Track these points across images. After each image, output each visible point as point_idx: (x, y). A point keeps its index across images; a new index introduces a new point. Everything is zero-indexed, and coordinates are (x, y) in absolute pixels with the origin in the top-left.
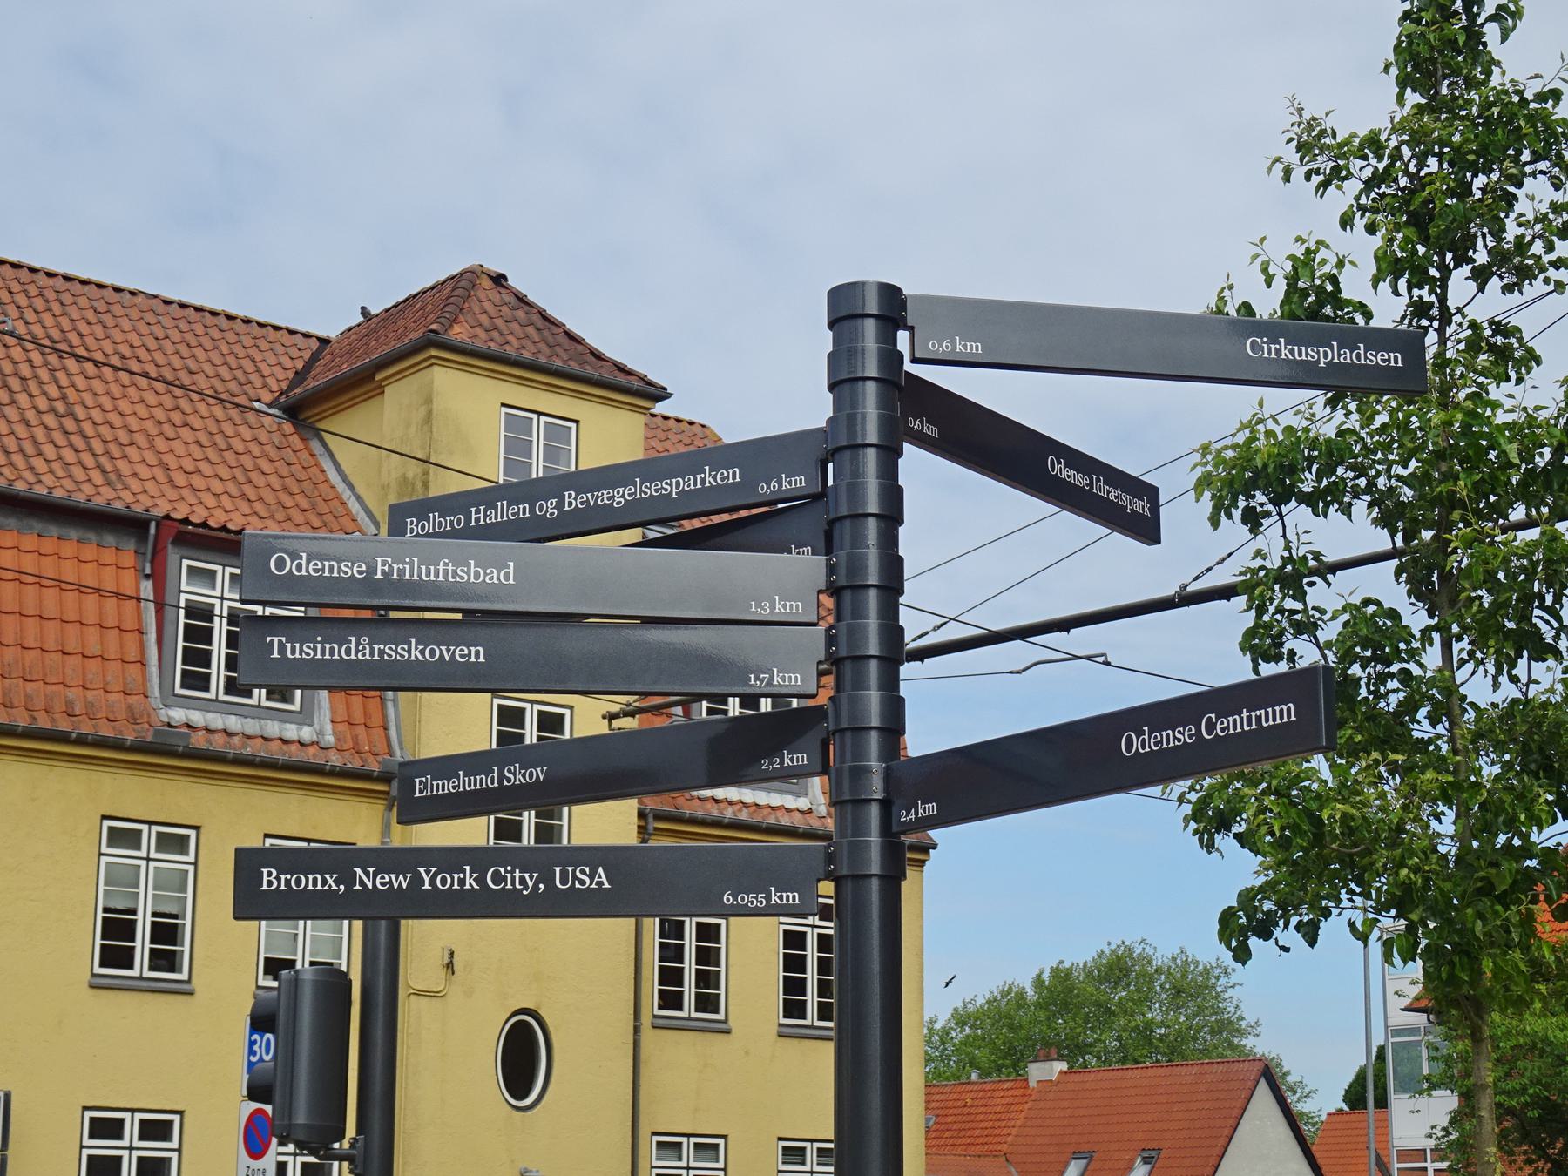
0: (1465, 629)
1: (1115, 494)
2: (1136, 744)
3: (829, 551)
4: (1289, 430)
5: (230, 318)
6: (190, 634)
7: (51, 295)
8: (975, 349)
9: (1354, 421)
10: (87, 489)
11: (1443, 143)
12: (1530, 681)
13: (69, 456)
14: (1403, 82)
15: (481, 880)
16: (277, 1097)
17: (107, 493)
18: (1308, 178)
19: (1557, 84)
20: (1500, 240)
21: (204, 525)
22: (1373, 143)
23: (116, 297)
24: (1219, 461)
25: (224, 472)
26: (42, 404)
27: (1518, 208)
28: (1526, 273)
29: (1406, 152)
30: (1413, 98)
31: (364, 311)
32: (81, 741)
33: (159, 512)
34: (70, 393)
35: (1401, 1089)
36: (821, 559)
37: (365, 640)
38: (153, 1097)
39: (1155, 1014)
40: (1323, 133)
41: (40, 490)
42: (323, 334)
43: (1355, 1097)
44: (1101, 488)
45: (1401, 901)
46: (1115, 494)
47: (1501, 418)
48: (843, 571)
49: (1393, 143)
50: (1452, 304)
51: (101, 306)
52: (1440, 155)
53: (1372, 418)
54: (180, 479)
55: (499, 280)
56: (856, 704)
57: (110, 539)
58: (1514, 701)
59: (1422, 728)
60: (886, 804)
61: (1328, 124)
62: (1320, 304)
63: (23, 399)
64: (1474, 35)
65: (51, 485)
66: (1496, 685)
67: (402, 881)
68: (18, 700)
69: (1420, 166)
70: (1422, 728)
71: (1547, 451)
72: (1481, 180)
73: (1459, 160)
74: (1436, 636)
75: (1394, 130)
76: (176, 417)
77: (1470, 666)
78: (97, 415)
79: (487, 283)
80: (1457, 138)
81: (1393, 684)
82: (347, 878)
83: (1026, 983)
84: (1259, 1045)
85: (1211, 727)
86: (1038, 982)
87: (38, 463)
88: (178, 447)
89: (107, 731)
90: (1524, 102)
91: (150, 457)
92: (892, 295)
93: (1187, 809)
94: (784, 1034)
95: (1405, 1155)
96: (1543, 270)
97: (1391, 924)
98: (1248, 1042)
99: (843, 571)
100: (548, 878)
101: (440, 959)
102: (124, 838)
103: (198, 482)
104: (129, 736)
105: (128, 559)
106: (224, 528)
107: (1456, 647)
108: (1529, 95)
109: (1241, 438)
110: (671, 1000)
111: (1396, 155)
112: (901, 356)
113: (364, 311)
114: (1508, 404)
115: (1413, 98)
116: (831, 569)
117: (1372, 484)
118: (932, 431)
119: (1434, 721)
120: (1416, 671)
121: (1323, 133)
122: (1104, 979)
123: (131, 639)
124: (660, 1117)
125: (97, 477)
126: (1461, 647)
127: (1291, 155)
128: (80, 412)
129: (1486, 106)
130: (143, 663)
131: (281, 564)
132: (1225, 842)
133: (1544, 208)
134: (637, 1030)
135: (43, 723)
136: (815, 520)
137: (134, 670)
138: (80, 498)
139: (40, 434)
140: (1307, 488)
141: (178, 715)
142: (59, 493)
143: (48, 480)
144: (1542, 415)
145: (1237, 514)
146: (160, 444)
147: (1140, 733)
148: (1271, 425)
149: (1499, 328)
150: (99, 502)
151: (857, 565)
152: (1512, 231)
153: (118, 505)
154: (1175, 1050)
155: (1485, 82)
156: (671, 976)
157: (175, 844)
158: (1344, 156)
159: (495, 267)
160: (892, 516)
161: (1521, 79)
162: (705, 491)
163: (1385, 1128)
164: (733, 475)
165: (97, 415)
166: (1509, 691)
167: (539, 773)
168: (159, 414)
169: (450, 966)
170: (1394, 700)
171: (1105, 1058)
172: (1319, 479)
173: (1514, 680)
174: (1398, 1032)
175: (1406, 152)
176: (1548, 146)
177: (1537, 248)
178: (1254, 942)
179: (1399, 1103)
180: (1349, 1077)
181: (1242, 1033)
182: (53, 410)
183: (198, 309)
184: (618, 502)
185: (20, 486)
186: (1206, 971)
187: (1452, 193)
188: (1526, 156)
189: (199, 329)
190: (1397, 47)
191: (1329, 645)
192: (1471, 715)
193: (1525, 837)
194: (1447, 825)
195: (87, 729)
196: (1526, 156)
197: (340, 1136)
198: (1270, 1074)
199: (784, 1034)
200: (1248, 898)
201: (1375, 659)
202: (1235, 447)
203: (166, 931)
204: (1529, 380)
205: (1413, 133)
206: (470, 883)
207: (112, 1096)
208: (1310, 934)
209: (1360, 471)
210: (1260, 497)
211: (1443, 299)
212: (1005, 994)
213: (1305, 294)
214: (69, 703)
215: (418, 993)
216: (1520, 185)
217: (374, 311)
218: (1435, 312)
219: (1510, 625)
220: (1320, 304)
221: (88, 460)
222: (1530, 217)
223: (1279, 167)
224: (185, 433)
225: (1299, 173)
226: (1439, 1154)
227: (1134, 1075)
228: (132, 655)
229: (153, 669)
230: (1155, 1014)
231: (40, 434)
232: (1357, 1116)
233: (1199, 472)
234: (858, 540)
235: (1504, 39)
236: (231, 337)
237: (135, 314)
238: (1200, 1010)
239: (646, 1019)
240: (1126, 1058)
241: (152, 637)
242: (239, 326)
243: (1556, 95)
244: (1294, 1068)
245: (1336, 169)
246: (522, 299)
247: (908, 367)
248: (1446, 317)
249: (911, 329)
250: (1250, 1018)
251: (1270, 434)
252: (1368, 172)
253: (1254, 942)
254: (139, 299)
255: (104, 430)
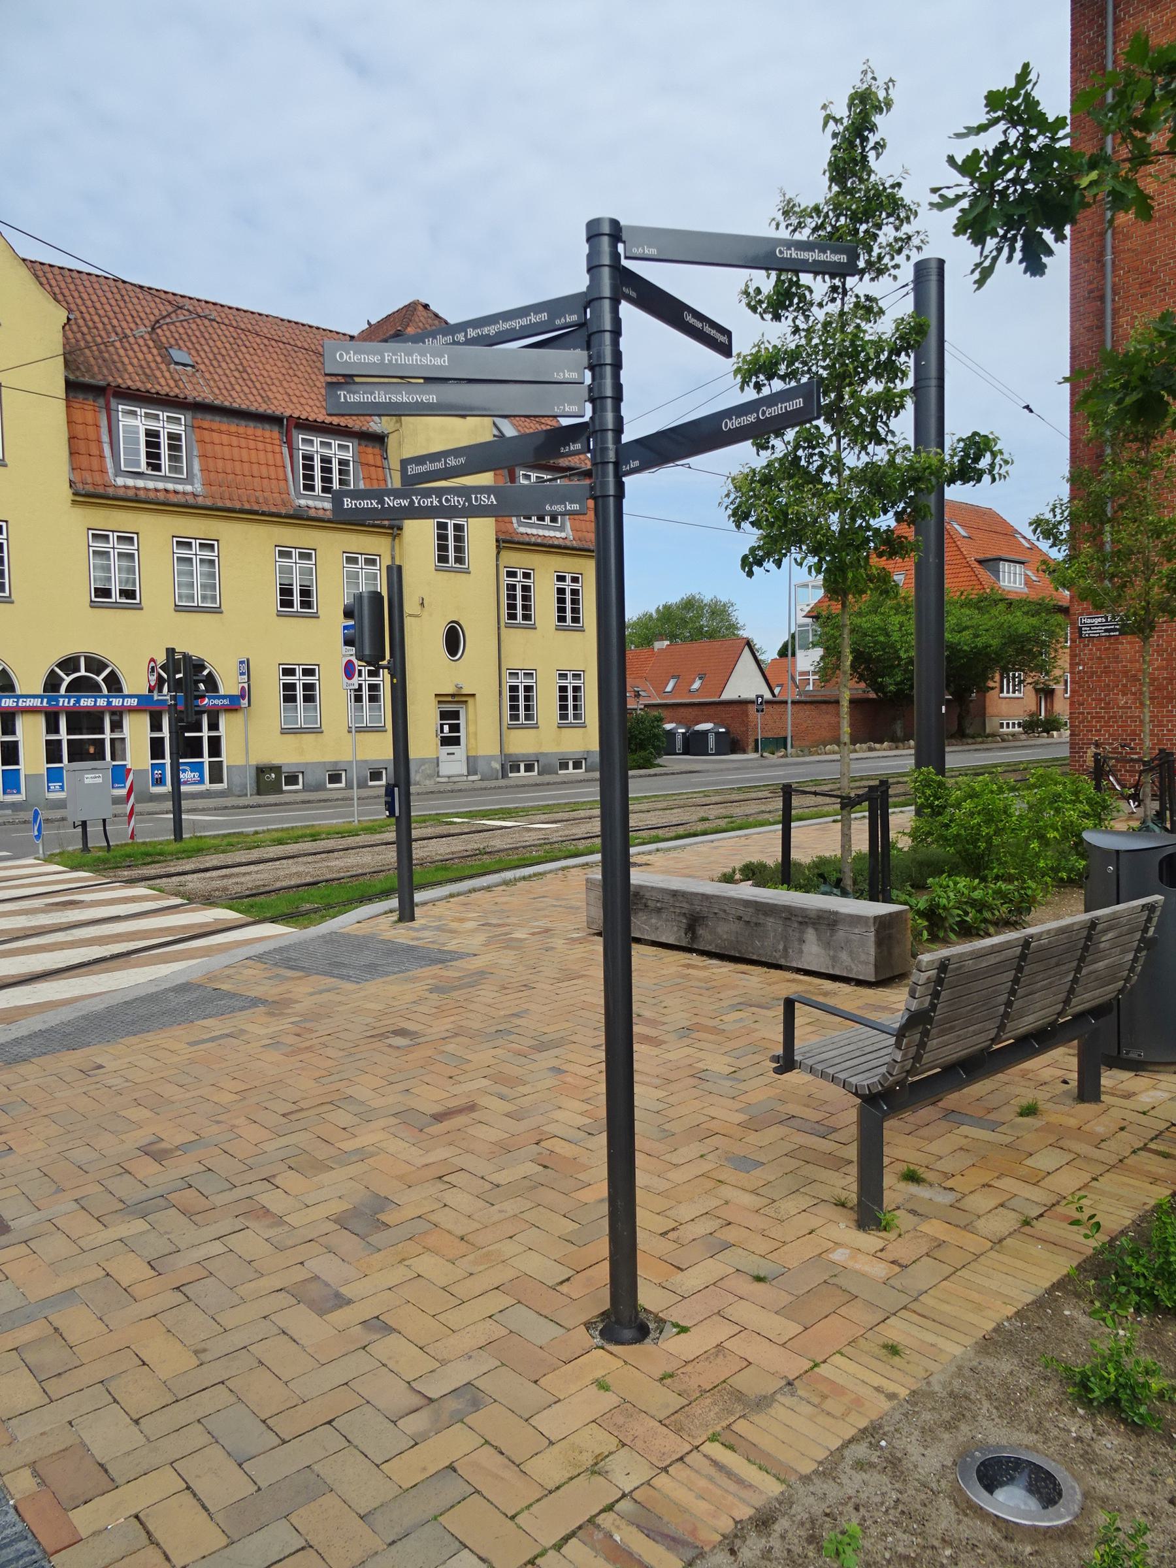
0: (846, 434)
1: (713, 332)
2: (729, 425)
3: (588, 348)
4: (775, 347)
5: (310, 327)
6: (305, 467)
7: (231, 317)
8: (652, 252)
9: (803, 342)
10: (255, 404)
11: (848, 209)
12: (875, 454)
13: (246, 389)
14: (832, 180)
15: (440, 502)
16: (357, 644)
17: (264, 406)
18: (787, 227)
19: (900, 180)
20: (870, 256)
21: (307, 419)
22: (817, 209)
23: (259, 318)
24: (745, 361)
25: (313, 396)
26: (232, 366)
27: (879, 240)
28: (880, 272)
29: (831, 214)
30: (835, 188)
31: (369, 323)
32: (263, 514)
33: (287, 414)
34: (244, 362)
35: (801, 648)
36: (586, 353)
37: (382, 393)
38: (307, 660)
39: (703, 622)
40: (794, 205)
41: (235, 405)
42: (352, 334)
43: (783, 653)
44: (707, 329)
45: (814, 551)
46: (713, 332)
47: (867, 338)
48: (595, 357)
49: (825, 210)
50: (848, 286)
51: (253, 322)
52: (846, 215)
53: (811, 340)
54: (295, 399)
55: (426, 306)
56: (603, 420)
57: (267, 426)
58: (867, 463)
59: (826, 478)
60: (617, 464)
61: (796, 201)
62: (790, 286)
63: (224, 365)
64: (864, 158)
65: (240, 403)
66: (859, 458)
67: (405, 503)
68: (235, 497)
69: (837, 221)
70: (826, 478)
71: (886, 353)
72: (863, 227)
73: (855, 218)
74: (834, 438)
75: (826, 203)
76: (291, 372)
77: (847, 451)
78: (256, 371)
79: (421, 308)
80: (854, 207)
81: (816, 458)
82: (382, 502)
83: (653, 611)
84: (744, 633)
85: (764, 413)
86: (658, 610)
87: (233, 393)
88: (292, 385)
89: (274, 510)
90: (885, 189)
91: (280, 389)
92: (615, 223)
93: (730, 512)
94: (558, 629)
95: (802, 674)
96: (888, 270)
97: (812, 560)
98: (741, 632)
99: (595, 357)
100: (469, 500)
101: (417, 601)
102: (285, 554)
103: (303, 401)
104: (283, 512)
105: (276, 435)
106: (315, 421)
107: (842, 441)
108: (887, 185)
109: (754, 351)
110: (512, 616)
111: (827, 214)
112: (619, 255)
113: (369, 323)
114: (870, 331)
115: (835, 188)
116: (590, 357)
117: (810, 370)
118: (633, 294)
119: (832, 473)
120: (826, 452)
121: (794, 205)
122: (683, 608)
123: (280, 470)
124: (511, 662)
125: (259, 399)
126: (844, 442)
127: (780, 217)
128: (249, 370)
129: (867, 191)
130: (286, 480)
131: (341, 356)
132: (746, 525)
133: (891, 240)
134: (499, 628)
135: (247, 507)
136: (583, 333)
137: (282, 483)
138: (253, 409)
139: (233, 380)
140: (782, 373)
141: (303, 502)
142: (244, 407)
143: (238, 400)
144: (884, 337)
145: (751, 385)
146: (284, 383)
147: (731, 419)
148: (767, 345)
149: (868, 298)
150: (261, 410)
151: (600, 355)
152: (876, 251)
153: (269, 411)
154: (712, 635)
155: (867, 180)
156: (512, 607)
157: (305, 556)
158: (803, 216)
159: (424, 301)
160: (617, 332)
161: (884, 177)
162: (531, 325)
163: (794, 664)
164: (544, 316)
165: (256, 371)
166: (865, 458)
167: (462, 460)
168: (284, 371)
169: (422, 604)
170: (816, 465)
171: (684, 640)
172: (787, 367)
173: (868, 454)
174: (800, 626)
175: (831, 214)
176: (894, 210)
177: (886, 260)
178: (755, 568)
179: (800, 654)
180: (779, 645)
181: (738, 629)
182: (237, 370)
183: (296, 323)
184: (492, 332)
185: (227, 404)
186: (724, 605)
187: (850, 234)
188: (884, 215)
189: (298, 332)
190: (830, 164)
191: (789, 443)
192: (847, 472)
193: (867, 522)
194: (834, 518)
195: (265, 509)
196: (884, 215)
197: (384, 659)
198: (749, 644)
199: (558, 629)
200: (753, 550)
201: (809, 447)
202: (751, 354)
203: (306, 593)
204: (879, 321)
205: (834, 204)
206: (436, 503)
207: (290, 660)
208: (779, 564)
209: (805, 363)
210: (762, 377)
211: (844, 284)
212: (645, 615)
213: (784, 282)
214: (257, 498)
215: (410, 615)
216: (880, 229)
217: (373, 322)
218: (840, 290)
219: (868, 430)
220: (790, 286)
221: (255, 391)
222: (884, 244)
223: (774, 223)
224: (295, 379)
225: (783, 225)
226: (815, 673)
227: (696, 645)
228: (279, 463)
229: (291, 483)
230: (703, 622)
231: (233, 380)
232: (783, 660)
233: (735, 366)
234: (601, 344)
235: (877, 158)
236: (312, 336)
237: (269, 325)
238: (722, 620)
239: (502, 624)
240: (692, 639)
241: (289, 469)
242: (314, 330)
243: (899, 185)
244: (758, 643)
245: (800, 223)
246: (436, 316)
247: (625, 263)
248: (845, 293)
249: (624, 242)
250: (741, 623)
251: (766, 349)
252: (813, 225)
253: (755, 568)
254: (270, 319)
255: (260, 378)
